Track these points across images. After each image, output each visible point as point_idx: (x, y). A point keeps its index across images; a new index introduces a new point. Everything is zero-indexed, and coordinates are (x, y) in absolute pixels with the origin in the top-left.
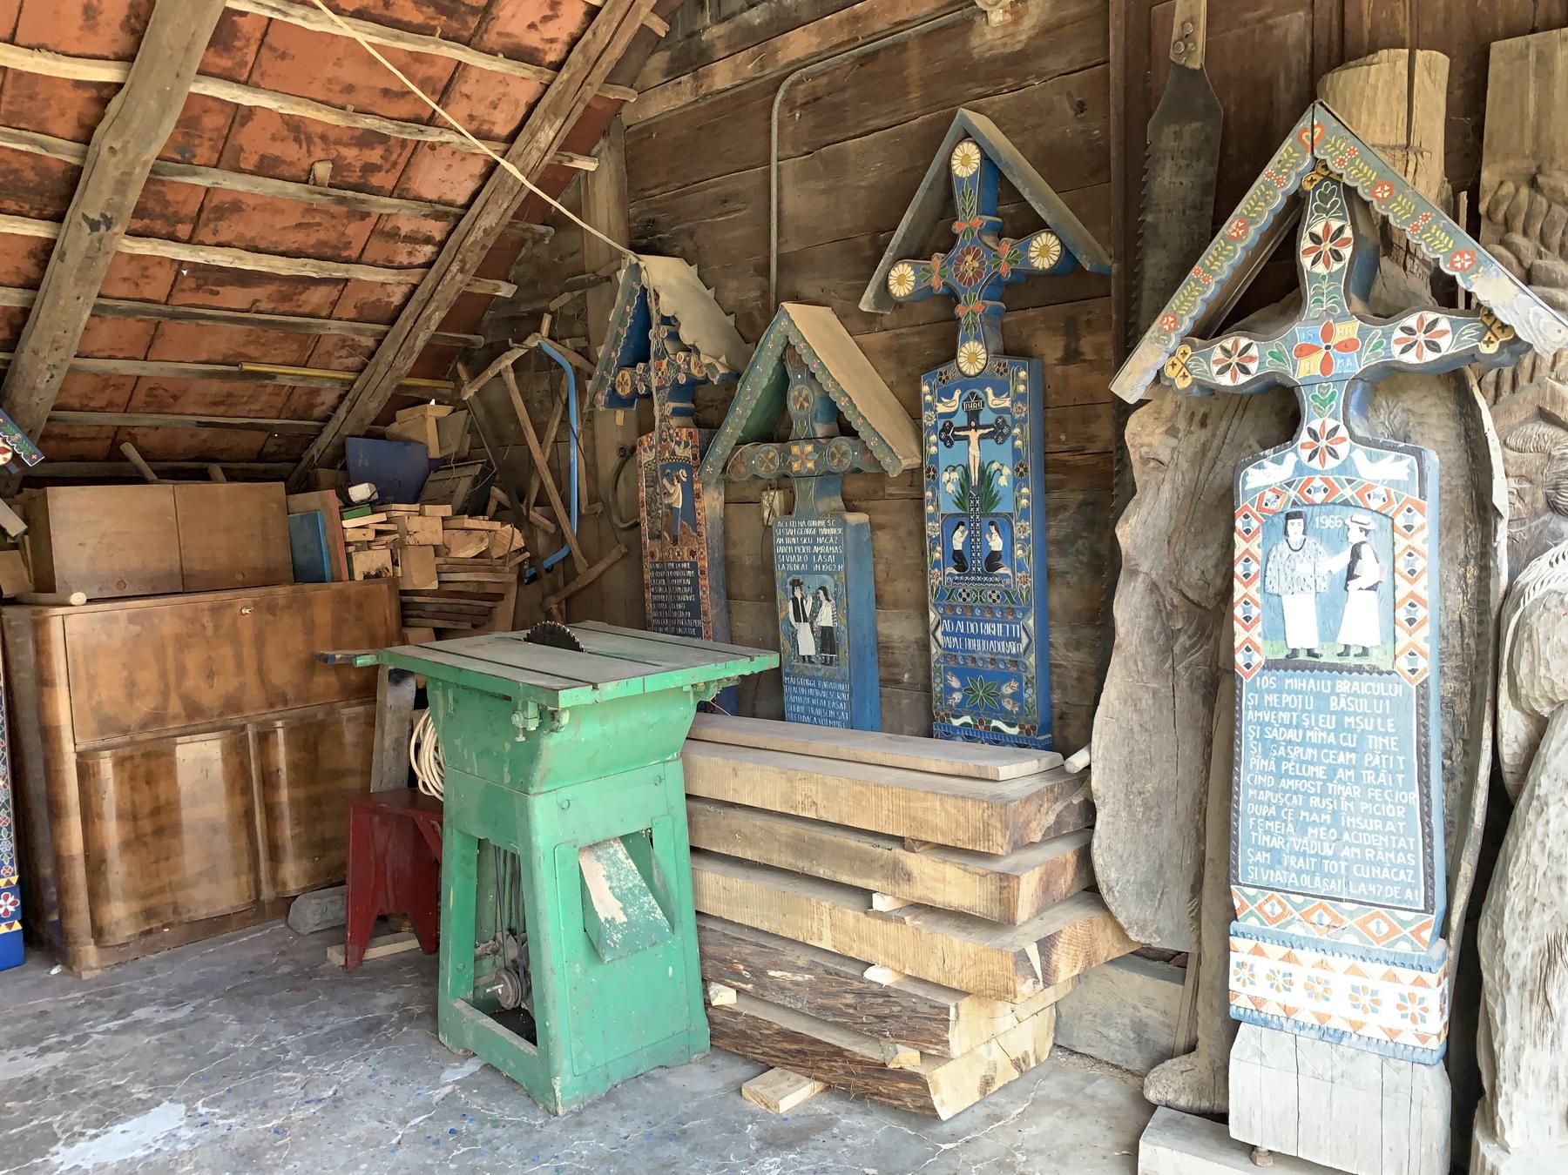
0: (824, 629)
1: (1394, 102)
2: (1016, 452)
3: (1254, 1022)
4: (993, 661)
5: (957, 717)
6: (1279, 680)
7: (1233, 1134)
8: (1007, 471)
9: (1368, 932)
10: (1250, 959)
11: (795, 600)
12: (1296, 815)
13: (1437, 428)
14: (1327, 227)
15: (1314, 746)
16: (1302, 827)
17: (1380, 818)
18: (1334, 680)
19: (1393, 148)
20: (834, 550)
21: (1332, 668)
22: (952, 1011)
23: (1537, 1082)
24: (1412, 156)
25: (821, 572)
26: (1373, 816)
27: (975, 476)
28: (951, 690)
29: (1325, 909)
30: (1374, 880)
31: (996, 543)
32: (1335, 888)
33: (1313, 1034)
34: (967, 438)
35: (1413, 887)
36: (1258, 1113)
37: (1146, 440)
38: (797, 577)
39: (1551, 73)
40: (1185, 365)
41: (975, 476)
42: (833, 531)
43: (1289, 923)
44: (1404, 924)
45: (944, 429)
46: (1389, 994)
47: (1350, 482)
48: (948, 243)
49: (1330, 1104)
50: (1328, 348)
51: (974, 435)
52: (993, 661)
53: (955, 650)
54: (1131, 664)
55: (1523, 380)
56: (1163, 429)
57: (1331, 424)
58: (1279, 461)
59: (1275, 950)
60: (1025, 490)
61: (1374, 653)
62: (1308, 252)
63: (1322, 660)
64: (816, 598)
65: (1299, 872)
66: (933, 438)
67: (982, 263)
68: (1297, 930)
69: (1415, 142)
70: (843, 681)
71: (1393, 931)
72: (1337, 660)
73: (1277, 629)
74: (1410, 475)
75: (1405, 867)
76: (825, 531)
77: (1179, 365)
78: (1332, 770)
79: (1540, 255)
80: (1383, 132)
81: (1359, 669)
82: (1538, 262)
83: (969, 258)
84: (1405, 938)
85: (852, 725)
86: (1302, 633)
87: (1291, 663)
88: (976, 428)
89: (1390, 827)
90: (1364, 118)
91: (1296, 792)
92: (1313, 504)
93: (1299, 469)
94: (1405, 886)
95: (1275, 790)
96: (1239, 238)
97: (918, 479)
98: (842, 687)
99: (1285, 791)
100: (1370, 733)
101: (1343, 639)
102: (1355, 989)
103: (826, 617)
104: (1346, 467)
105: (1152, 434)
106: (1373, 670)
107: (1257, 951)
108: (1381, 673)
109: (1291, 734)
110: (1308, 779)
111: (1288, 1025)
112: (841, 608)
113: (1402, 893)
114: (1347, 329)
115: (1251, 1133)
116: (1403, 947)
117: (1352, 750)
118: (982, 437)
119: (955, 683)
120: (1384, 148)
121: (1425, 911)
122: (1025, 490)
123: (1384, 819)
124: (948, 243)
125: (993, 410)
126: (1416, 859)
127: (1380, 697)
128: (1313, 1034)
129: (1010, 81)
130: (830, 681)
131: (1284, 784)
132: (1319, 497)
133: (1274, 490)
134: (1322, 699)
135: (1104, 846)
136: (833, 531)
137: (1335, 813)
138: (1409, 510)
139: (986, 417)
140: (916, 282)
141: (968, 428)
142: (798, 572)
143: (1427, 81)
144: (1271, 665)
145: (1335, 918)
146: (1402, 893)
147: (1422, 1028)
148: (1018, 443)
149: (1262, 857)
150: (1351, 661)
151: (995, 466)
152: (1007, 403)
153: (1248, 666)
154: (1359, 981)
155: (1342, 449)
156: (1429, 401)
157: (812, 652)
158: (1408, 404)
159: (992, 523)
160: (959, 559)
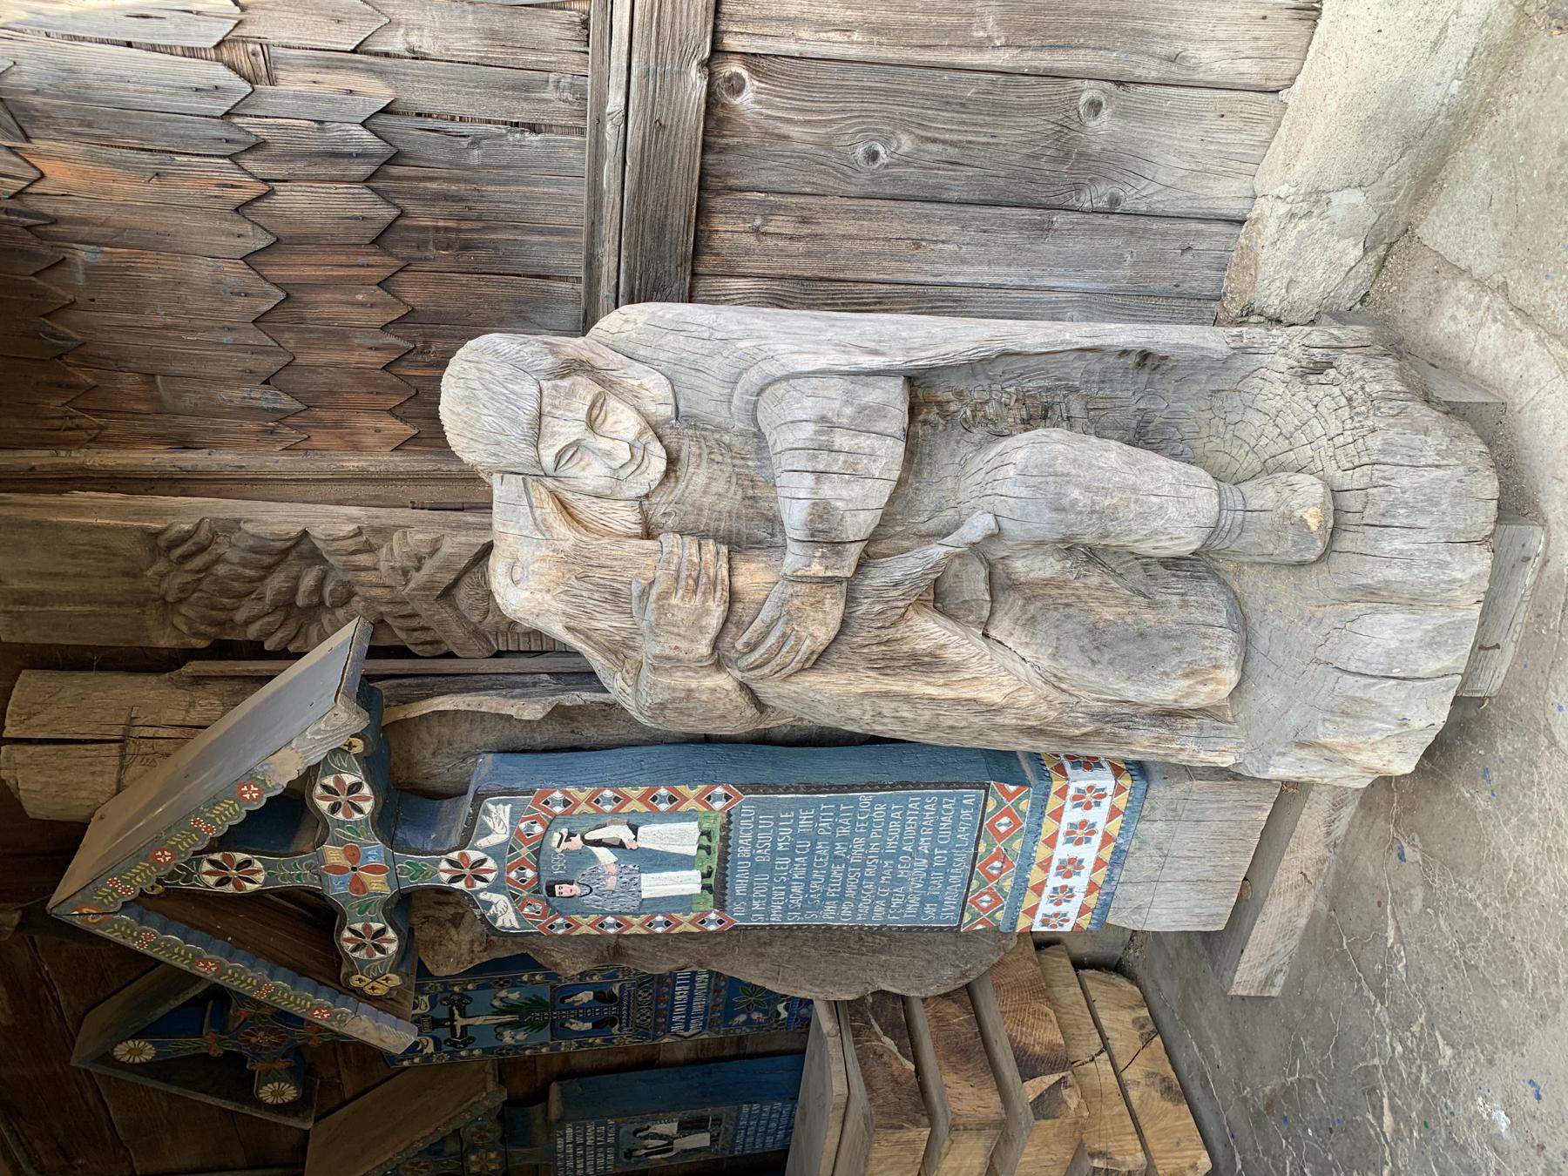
0: (680, 1127)
1: (66, 762)
2: (479, 988)
3: (1105, 914)
4: (717, 991)
5: (779, 1014)
6: (736, 899)
7: (1221, 927)
8: (503, 994)
9: (1008, 832)
10: (1039, 916)
11: (647, 1154)
12: (884, 886)
13: (455, 728)
14: (209, 873)
15: (809, 873)
16: (896, 881)
17: (887, 823)
18: (735, 860)
19: (123, 757)
20: (590, 1128)
21: (723, 859)
22: (1097, 1163)
23: (1166, 740)
24: (136, 732)
25: (617, 1137)
26: (886, 828)
27: (508, 1018)
28: (749, 1022)
29: (986, 864)
30: (954, 828)
31: (586, 996)
32: (962, 860)
33: (1117, 871)
34: (464, 1028)
35: (961, 798)
36: (1198, 910)
37: (465, 947)
38: (621, 1154)
39: (42, 594)
40: (374, 979)
41: (508, 1018)
42: (569, 1131)
43: (1001, 890)
44: (1000, 804)
45: (455, 1044)
46: (1072, 815)
47: (512, 850)
48: (235, 1060)
49: (1188, 858)
50: (354, 869)
51: (460, 1022)
52: (717, 991)
53: (704, 1021)
54: (719, 949)
55: (407, 610)
56: (453, 931)
57: (444, 865)
58: (489, 904)
59: (1029, 899)
60: (525, 978)
61: (706, 826)
62: (238, 886)
63: (714, 866)
64: (646, 1138)
65: (946, 883)
66: (463, 1053)
67: (260, 1029)
68: (1008, 884)
69: (116, 733)
70: (740, 1109)
71: (1008, 813)
72: (715, 856)
73: (684, 902)
74: (505, 803)
75: (940, 804)
76: (569, 1138)
77: (375, 984)
78: (835, 859)
79: (260, 599)
80: (102, 773)
81: (725, 839)
82: (267, 600)
83: (253, 1040)
84: (1016, 805)
85: (791, 1093)
86: (688, 882)
87: (717, 887)
88: (452, 1019)
89: (897, 815)
90: (84, 794)
91: (860, 885)
92: (538, 877)
93: (494, 889)
94: (959, 805)
95: (857, 900)
96: (219, 965)
97: (507, 1066)
98: (745, 1109)
99: (859, 893)
100: (795, 829)
101: (692, 850)
102: (1068, 841)
103: (670, 1128)
104: (492, 851)
105: (458, 944)
106: (726, 827)
107: (1031, 912)
108: (730, 822)
109: (797, 889)
110: (845, 877)
111: (1107, 889)
112: (659, 1114)
113: (967, 807)
114: (333, 854)
115: (1221, 910)
116: (1025, 805)
117: (814, 844)
118: (463, 1015)
119: (742, 1018)
120: (122, 768)
121: (987, 790)
122: (525, 978)
123: (888, 819)
124: (235, 1060)
125: (433, 1007)
126: (931, 795)
127: (756, 823)
128: (1117, 871)
129: (43, 991)
130: (738, 1119)
131: (850, 892)
132: (530, 873)
133: (522, 908)
134: (756, 868)
135: (916, 982)
136: (569, 1131)
137: (882, 857)
138: (547, 803)
139: (441, 1012)
140: (280, 1081)
141: (453, 1028)
142: (616, 1155)
143: (44, 717)
144: (721, 904)
145: (995, 858)
146: (967, 807)
147: (1110, 790)
148: (470, 987)
149: (930, 909)
150: (715, 844)
151: (496, 1003)
152: (426, 998)
153: (721, 922)
154: (1061, 838)
155: (474, 855)
156: (425, 736)
157: (708, 1136)
158: (428, 754)
159: (562, 1001)
160: (600, 1025)
